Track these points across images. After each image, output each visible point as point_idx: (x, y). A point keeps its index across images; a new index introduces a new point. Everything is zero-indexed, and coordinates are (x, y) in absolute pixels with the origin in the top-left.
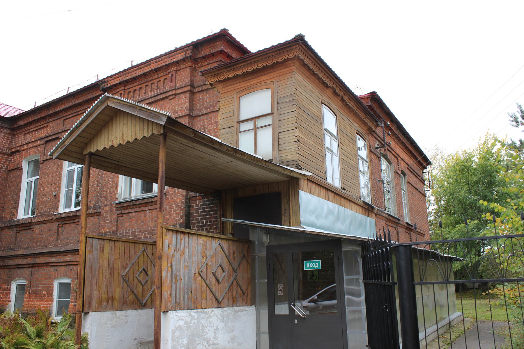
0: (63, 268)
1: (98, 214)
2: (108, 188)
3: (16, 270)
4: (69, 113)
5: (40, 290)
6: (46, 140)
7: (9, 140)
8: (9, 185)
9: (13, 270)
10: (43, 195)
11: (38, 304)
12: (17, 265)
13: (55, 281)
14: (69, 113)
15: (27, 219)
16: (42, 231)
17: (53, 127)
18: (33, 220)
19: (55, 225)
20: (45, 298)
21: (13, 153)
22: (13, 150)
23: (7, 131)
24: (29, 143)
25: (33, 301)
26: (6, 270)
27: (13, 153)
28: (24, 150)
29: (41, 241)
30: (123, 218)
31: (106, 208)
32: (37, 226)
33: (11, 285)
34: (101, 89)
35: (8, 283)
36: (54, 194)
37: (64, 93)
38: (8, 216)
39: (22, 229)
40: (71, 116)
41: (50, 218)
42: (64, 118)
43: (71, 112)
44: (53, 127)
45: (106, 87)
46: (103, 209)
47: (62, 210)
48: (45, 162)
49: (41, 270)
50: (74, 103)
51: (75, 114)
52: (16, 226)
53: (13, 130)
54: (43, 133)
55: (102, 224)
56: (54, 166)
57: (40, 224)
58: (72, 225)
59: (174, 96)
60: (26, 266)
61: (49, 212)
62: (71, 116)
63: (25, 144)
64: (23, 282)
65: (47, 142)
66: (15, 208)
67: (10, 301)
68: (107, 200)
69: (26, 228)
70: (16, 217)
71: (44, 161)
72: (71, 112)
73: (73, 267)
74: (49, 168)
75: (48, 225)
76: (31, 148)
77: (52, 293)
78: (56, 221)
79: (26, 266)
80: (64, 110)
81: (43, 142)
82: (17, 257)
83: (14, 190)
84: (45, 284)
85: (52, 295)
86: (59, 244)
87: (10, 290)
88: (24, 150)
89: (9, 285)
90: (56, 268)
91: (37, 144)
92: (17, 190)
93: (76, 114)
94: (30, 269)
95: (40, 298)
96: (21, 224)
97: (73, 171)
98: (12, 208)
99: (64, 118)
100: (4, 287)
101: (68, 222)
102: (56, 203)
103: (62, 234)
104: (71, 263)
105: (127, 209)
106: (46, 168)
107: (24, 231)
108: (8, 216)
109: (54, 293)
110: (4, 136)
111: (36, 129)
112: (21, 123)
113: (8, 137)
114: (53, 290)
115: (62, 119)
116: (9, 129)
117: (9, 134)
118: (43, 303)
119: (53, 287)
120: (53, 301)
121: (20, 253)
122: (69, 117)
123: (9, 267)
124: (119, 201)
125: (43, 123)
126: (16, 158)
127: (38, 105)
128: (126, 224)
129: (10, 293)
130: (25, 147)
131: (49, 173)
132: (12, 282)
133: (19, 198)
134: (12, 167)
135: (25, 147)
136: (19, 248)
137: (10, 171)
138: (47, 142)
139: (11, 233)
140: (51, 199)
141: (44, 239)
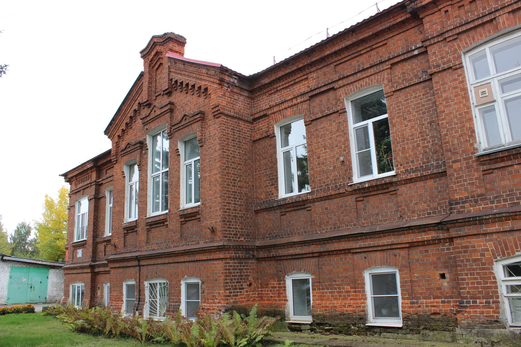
0: (379, 255)
1: (444, 174)
2: (454, 137)
3: (289, 261)
4: (343, 56)
5: (338, 285)
6: (310, 94)
7: (249, 104)
8: (256, 159)
9: (286, 263)
10: (319, 164)
11: (337, 303)
12: (292, 255)
13: (365, 271)
14: (343, 56)
15: (291, 198)
16: (326, 209)
17: (318, 77)
18: (310, 197)
19: (351, 200)
20: (349, 296)
21: (255, 120)
22: (257, 116)
23: (246, 94)
24: (283, 103)
25: (327, 299)
26: (273, 263)
27: (255, 120)
28: (274, 113)
29: (328, 222)
30: (494, 175)
31: (455, 166)
32: (316, 204)
33: (285, 281)
34: (409, 11)
35: (279, 277)
36: (342, 158)
37: (373, 12)
38: (263, 196)
39: (289, 209)
40: (346, 59)
41: (341, 191)
42: (335, 64)
43: (347, 54)
44: (318, 77)
45: (419, 6)
46: (451, 167)
47: (282, 194)
48: (314, 122)
49: (335, 259)
50: (354, 40)
51: (353, 56)
52: (280, 207)
53: (251, 92)
54: (302, 88)
55: (452, 187)
56: (331, 125)
57: (322, 200)
58: (381, 196)
59: (456, 37)
60: (308, 255)
61: (336, 183)
62: (346, 59)
63: (276, 105)
64: (132, 282)
65: (311, 97)
66: (273, 185)
67: (287, 301)
68: (453, 154)
69: (296, 208)
70: (277, 196)
71: (312, 121)
72: (347, 54)
73: (398, 251)
74: (322, 128)
75: (336, 201)
76: (286, 108)
77: (364, 288)
78: (352, 194)
79: (308, 255)
80: (336, 53)
81: (306, 97)
82: (293, 244)
83: (266, 164)
84: (346, 277)
85: (364, 291)
86: (364, 223)
87: (285, 287)
88: (274, 113)
89: (281, 280)
90: (363, 255)
91: (295, 102)
92: (272, 162)
93: (357, 54)
94: (316, 260)
95: (340, 296)
96: (289, 204)
97: (366, 128)
98: (268, 186)
99: (335, 64)
100: (274, 283)
101: (372, 194)
102: (346, 170)
103: (364, 210)
104: (394, 247)
105: (497, 162)
106: (316, 130)
107: (293, 213)
108: (263, 196)
109: (366, 287)
110: (244, 100)
111: (287, 85)
112: (266, 81)
113: (247, 101)
114: (364, 284)
115: (332, 66)
116: (248, 91)
117: (248, 97)
118: (348, 302)
119: (364, 280)
120: (366, 299)
121: (296, 239)
122: (343, 61)
123: (278, 259)
124: (481, 152)
125: (299, 76)
126: (262, 125)
127: (278, 61)
128: (503, 183)
129: (285, 290)
130: (276, 109)
131: (324, 135)
132: (286, 276)
133: (277, 172)
134: (258, 137)
135: (276, 109)
136: (292, 234)
137: (254, 141)
138: (311, 97)
139: (275, 215)
140: (334, 167)
141: (337, 219)
